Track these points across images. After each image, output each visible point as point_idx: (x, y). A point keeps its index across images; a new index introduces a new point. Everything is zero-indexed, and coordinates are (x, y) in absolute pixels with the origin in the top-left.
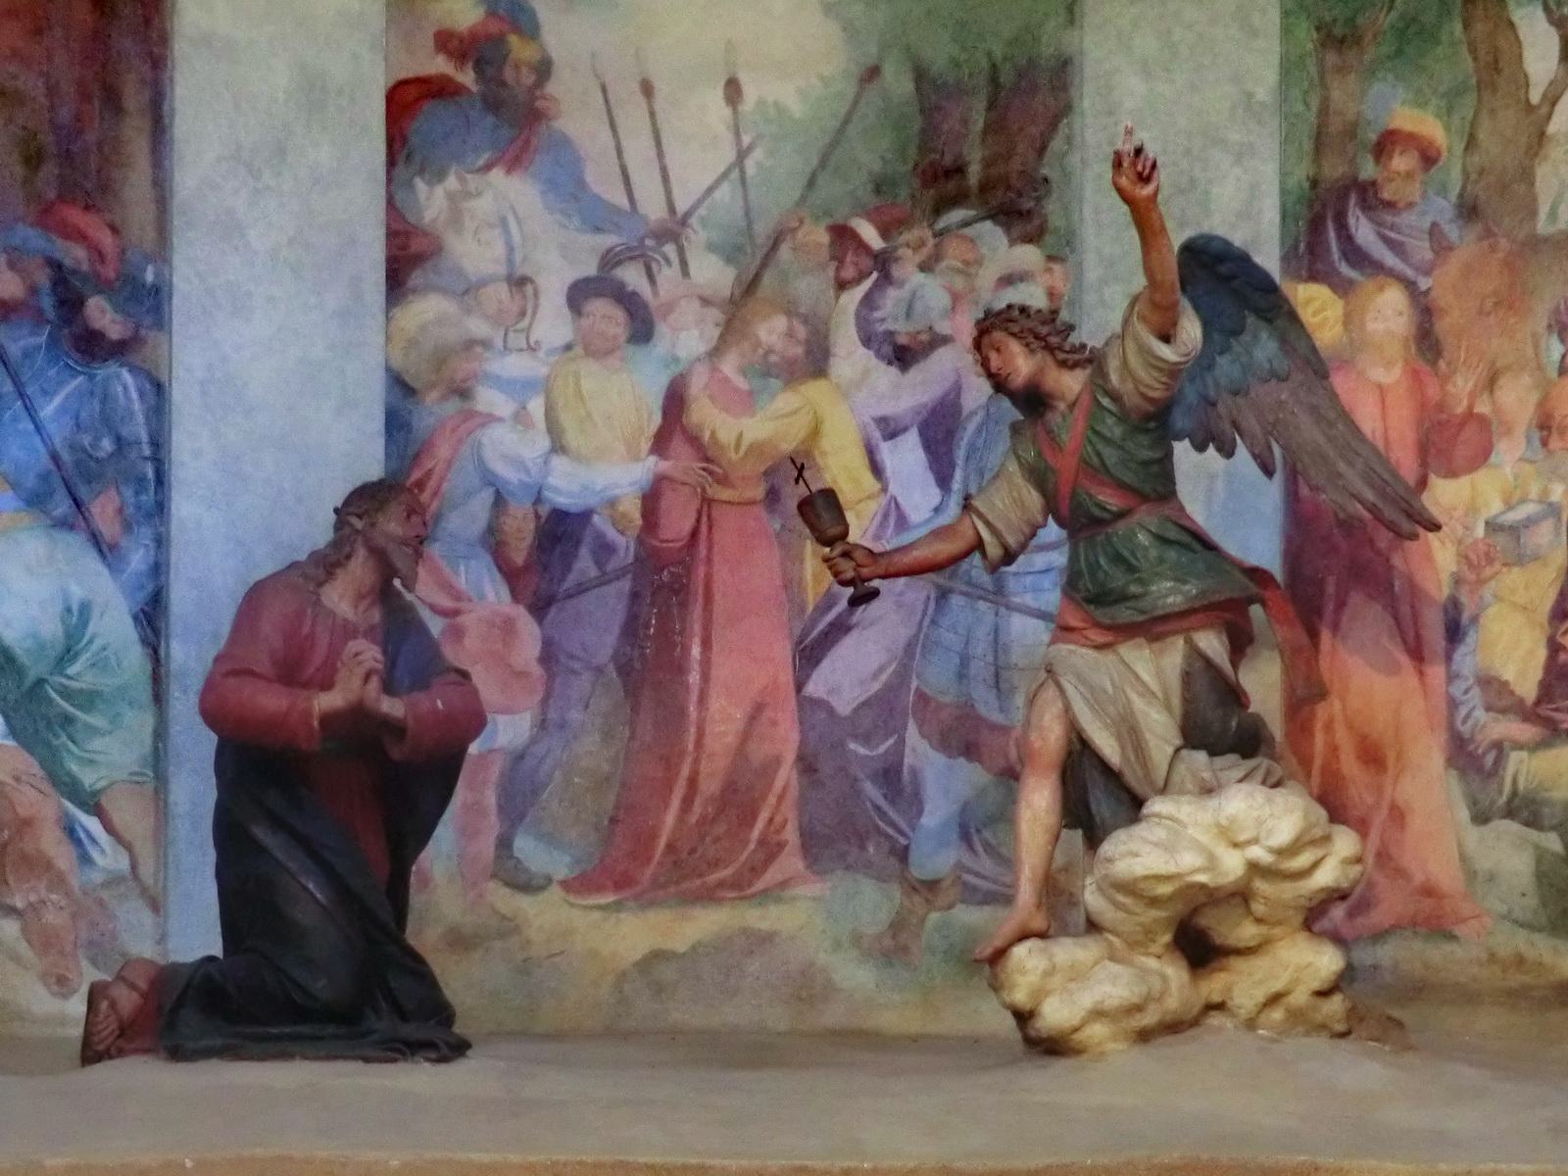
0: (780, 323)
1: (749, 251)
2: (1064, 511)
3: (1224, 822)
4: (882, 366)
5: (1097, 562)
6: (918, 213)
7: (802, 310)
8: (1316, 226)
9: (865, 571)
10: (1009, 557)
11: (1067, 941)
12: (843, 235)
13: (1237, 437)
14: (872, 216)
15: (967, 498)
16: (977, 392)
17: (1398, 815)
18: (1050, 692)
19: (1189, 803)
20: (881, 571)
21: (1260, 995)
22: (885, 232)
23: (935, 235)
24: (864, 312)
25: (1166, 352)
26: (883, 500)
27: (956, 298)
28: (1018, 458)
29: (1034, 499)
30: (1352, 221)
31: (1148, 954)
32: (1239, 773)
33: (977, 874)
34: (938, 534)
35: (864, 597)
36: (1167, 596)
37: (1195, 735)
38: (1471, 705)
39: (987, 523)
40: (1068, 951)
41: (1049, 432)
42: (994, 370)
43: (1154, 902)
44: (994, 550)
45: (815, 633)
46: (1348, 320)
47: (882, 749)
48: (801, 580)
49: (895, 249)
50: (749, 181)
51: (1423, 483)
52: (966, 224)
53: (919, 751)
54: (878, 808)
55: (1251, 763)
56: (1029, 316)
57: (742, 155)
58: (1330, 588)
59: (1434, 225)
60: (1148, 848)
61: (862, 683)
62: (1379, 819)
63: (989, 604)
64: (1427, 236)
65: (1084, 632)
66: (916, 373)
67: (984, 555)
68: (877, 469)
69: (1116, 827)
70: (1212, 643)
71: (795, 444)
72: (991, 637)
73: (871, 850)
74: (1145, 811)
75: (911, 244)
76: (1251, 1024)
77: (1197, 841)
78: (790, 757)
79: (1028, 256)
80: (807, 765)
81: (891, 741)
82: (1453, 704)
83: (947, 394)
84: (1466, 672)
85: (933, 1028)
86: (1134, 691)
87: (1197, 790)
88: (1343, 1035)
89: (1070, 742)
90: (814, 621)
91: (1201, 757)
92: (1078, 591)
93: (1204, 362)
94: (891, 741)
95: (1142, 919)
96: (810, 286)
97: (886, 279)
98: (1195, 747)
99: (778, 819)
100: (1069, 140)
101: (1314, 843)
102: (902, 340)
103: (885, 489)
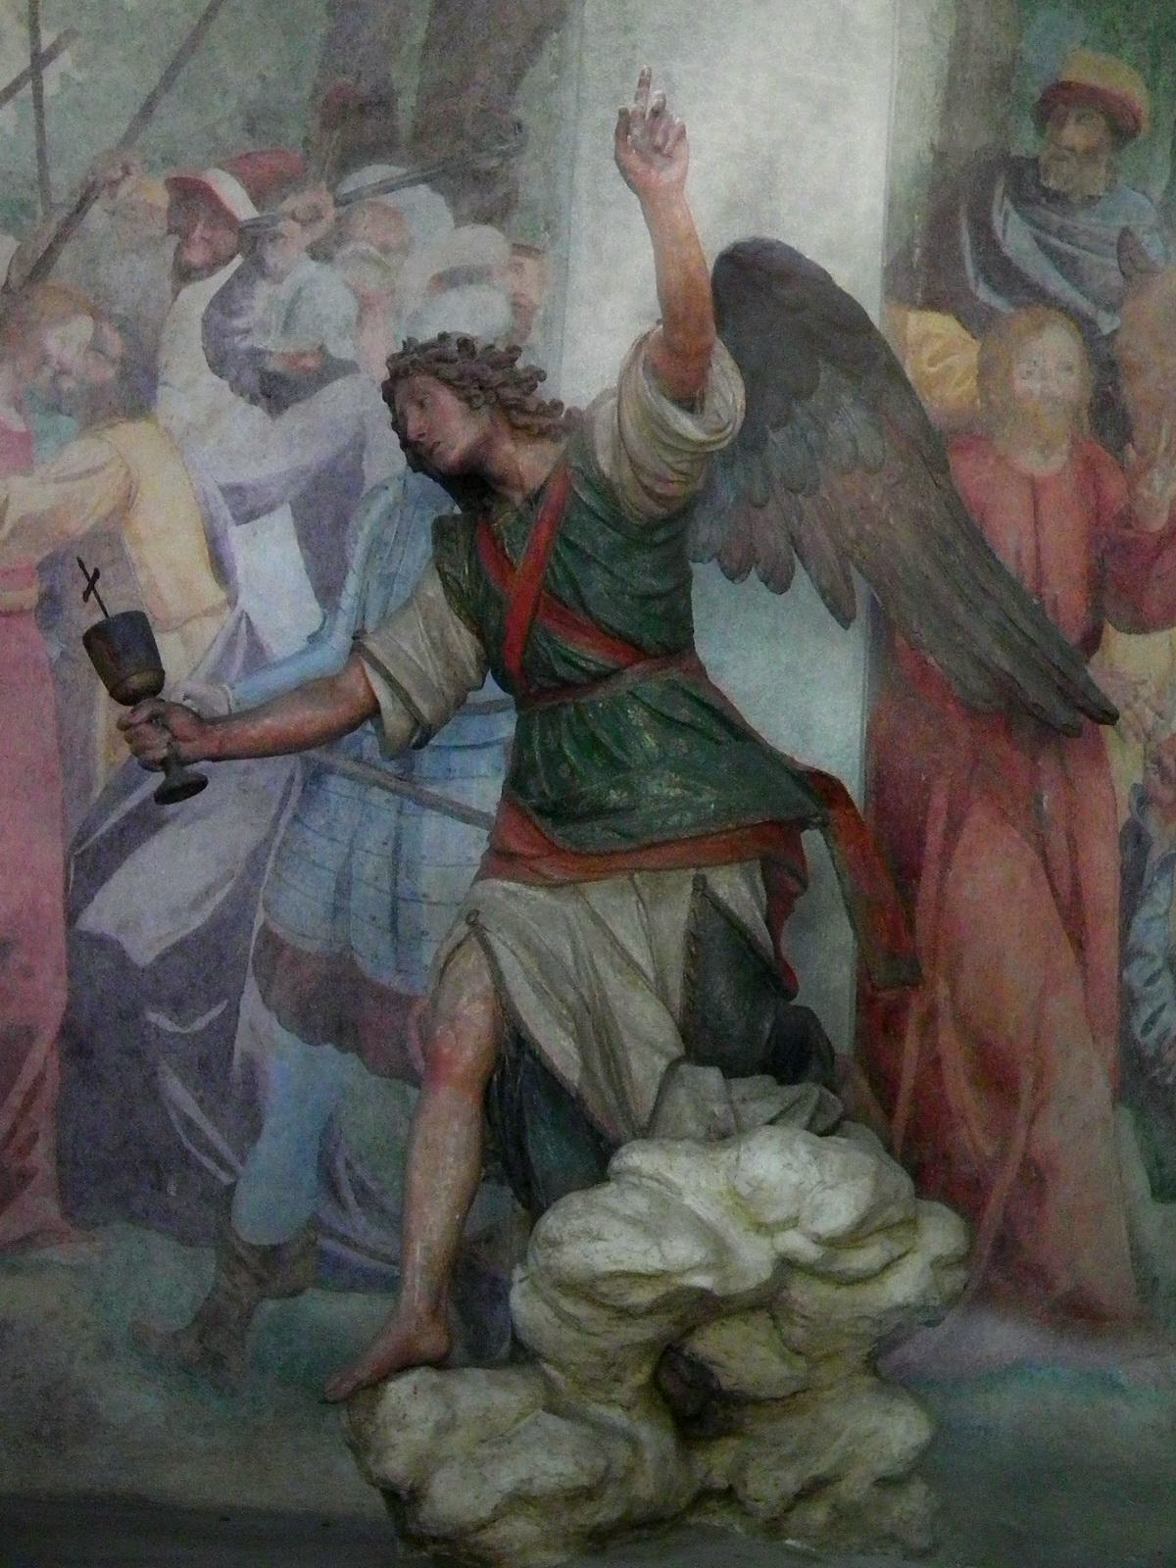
0: (82, 327)
1: (40, 213)
2: (513, 665)
3: (744, 1190)
4: (242, 404)
5: (560, 746)
6: (314, 168)
7: (118, 309)
8: (941, 224)
9: (185, 749)
10: (423, 734)
11: (479, 1374)
12: (190, 194)
13: (797, 561)
14: (239, 166)
15: (358, 636)
16: (386, 459)
17: (1035, 1176)
18: (472, 960)
19: (688, 1154)
20: (212, 748)
21: (790, 1480)
22: (258, 197)
23: (337, 203)
24: (218, 317)
25: (686, 425)
26: (229, 618)
27: (365, 304)
28: (443, 576)
29: (464, 643)
30: (997, 220)
31: (611, 1402)
32: (771, 1109)
33: (344, 1240)
34: (307, 690)
35: (182, 789)
36: (670, 812)
37: (701, 1039)
38: (1157, 1004)
39: (389, 678)
40: (481, 1394)
41: (495, 539)
42: (412, 436)
43: (625, 1314)
44: (395, 720)
45: (105, 828)
46: (984, 371)
47: (200, 1024)
48: (88, 740)
49: (274, 221)
50: (46, 102)
51: (1092, 641)
52: (387, 187)
53: (262, 1030)
54: (189, 1123)
55: (791, 1092)
56: (473, 354)
57: (40, 60)
58: (939, 801)
59: (1126, 232)
60: (617, 1226)
61: (174, 912)
62: (1004, 1182)
63: (387, 795)
64: (1114, 250)
65: (535, 864)
66: (294, 419)
67: (380, 726)
68: (220, 567)
69: (568, 1191)
70: (736, 889)
71: (91, 521)
72: (389, 848)
73: (172, 1189)
74: (615, 1164)
75: (300, 215)
76: (774, 1528)
77: (698, 1218)
78: (48, 1033)
79: (486, 243)
80: (76, 1043)
81: (215, 1012)
82: (1129, 1000)
83: (340, 455)
84: (1151, 947)
85: (257, 1497)
86: (608, 956)
87: (701, 1132)
88: (923, 1555)
89: (497, 1035)
90: (104, 808)
91: (712, 1077)
92: (527, 795)
93: (750, 439)
94: (215, 1012)
95: (602, 1344)
96: (135, 272)
97: (257, 267)
98: (703, 1061)
99: (24, 1132)
100: (559, 67)
101: (887, 1229)
102: (273, 365)
103: (232, 602)
